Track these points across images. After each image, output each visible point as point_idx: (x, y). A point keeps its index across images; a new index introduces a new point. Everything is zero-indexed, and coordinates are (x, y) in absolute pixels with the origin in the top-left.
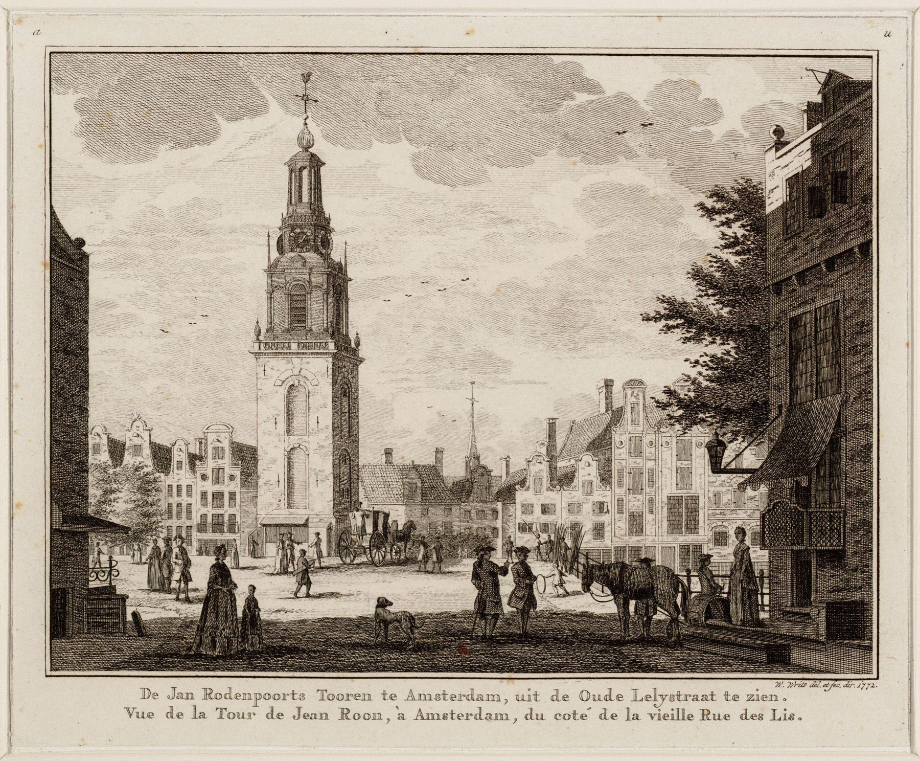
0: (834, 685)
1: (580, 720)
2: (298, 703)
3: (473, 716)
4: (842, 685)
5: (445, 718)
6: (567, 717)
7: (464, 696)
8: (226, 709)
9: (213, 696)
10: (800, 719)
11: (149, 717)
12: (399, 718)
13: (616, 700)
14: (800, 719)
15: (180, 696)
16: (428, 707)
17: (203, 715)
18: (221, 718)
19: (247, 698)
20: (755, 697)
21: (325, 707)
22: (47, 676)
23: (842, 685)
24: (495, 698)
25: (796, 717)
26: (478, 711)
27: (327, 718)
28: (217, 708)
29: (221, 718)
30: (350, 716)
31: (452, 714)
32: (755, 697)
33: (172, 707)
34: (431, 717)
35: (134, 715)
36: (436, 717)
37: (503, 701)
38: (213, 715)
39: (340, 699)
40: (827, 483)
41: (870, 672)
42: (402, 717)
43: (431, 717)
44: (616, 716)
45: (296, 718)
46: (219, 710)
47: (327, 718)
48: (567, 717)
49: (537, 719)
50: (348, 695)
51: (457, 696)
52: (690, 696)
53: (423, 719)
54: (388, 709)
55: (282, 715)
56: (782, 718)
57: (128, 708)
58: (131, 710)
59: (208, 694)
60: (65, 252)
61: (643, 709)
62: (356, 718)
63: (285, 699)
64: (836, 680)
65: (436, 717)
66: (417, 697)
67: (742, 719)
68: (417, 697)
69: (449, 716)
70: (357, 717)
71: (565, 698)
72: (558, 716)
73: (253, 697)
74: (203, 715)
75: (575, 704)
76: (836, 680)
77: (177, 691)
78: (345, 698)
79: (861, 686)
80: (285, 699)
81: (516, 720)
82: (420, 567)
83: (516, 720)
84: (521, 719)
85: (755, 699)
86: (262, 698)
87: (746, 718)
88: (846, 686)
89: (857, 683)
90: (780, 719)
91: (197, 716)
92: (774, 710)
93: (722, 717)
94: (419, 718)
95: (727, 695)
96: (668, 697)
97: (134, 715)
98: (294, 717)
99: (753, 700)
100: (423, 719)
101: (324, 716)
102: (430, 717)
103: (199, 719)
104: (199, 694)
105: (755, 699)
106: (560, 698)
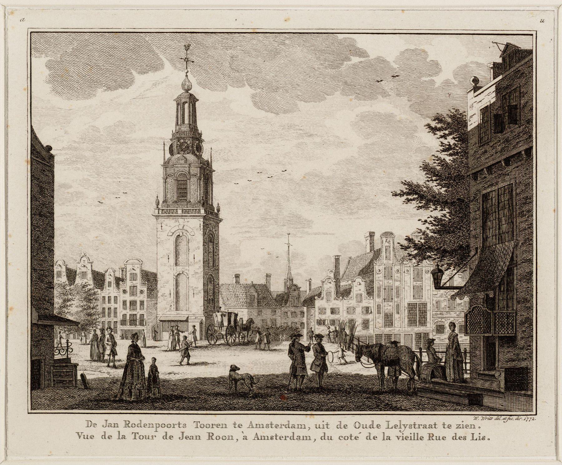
0: (509, 419)
1: (355, 440)
2: (182, 429)
4: (514, 419)
5: (272, 438)
6: (346, 438)
7: (284, 425)
8: (138, 433)
9: (130, 425)
10: (489, 439)
11: (91, 438)
12: (243, 439)
13: (376, 428)
14: (489, 439)
15: (110, 425)
16: (261, 432)
17: (124, 437)
18: (135, 438)
19: (151, 426)
20: (461, 426)
21: (199, 432)
22: (29, 413)
23: (514, 419)
24: (302, 427)
25: (486, 438)
26: (292, 435)
27: (200, 439)
28: (133, 433)
29: (135, 438)
30: (214, 437)
31: (276, 436)
32: (461, 426)
33: (105, 432)
34: (263, 438)
36: (266, 438)
37: (307, 429)
38: (130, 437)
39: (208, 427)
42: (245, 438)
43: (263, 438)
44: (377, 437)
46: (134, 434)
47: (200, 439)
48: (346, 438)
49: (328, 439)
50: (212, 425)
52: (422, 425)
53: (258, 439)
54: (237, 433)
55: (173, 437)
56: (478, 439)
57: (78, 433)
58: (80, 434)
62: (218, 438)
63: (174, 427)
64: (511, 415)
65: (266, 438)
66: (255, 426)
67: (453, 439)
68: (255, 426)
69: (274, 438)
70: (218, 438)
71: (345, 426)
72: (341, 437)
73: (154, 426)
74: (124, 437)
75: (351, 430)
76: (511, 415)
77: (108, 422)
78: (211, 426)
79: (526, 419)
80: (174, 427)
81: (315, 440)
82: (256, 346)
83: (315, 440)
84: (318, 440)
85: (461, 427)
86: (160, 427)
88: (517, 419)
89: (523, 417)
90: (476, 439)
91: (121, 437)
94: (256, 438)
95: (444, 425)
96: (408, 426)
97: (82, 437)
98: (180, 438)
99: (460, 428)
100: (258, 439)
101: (198, 437)
102: (263, 438)
103: (121, 440)
105: (461, 427)
106: (342, 427)
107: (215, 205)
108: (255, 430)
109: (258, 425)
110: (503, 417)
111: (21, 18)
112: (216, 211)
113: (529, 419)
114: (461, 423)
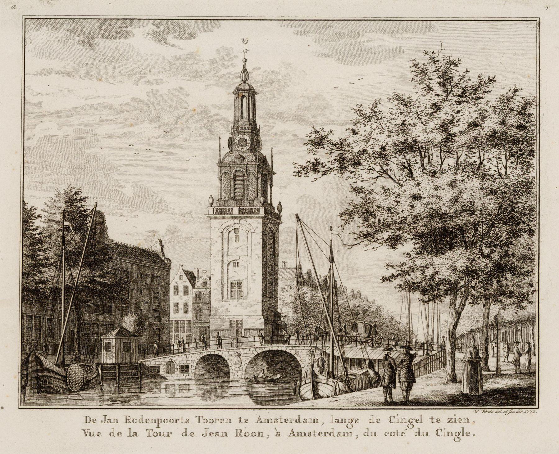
0: (510, 412)
1: (401, 436)
2: (185, 425)
3: (389, 434)
4: (515, 412)
5: (309, 435)
6: (393, 434)
9: (131, 421)
10: (474, 435)
11: (98, 436)
12: (276, 435)
13: (132, 423)
14: (474, 435)
15: (337, 421)
16: (213, 428)
17: (135, 434)
18: (149, 436)
20: (453, 420)
21: (261, 428)
22: (19, 409)
23: (515, 412)
24: (314, 421)
25: (472, 434)
26: (332, 431)
27: (226, 436)
28: (147, 430)
29: (149, 436)
30: (242, 434)
31: (314, 432)
32: (453, 420)
33: (114, 429)
34: (300, 434)
35: (88, 434)
36: (303, 434)
37: (321, 423)
38: (142, 433)
39: (172, 422)
40: (91, 331)
41: (535, 405)
42: (278, 434)
43: (300, 434)
44: (404, 433)
45: (205, 435)
47: (226, 436)
48: (393, 434)
49: (372, 436)
51: (289, 420)
53: (294, 435)
54: (106, 429)
55: (194, 434)
57: (84, 430)
58: (86, 431)
59: (127, 420)
60: (336, 295)
61: (140, 428)
62: (247, 435)
63: (216, 422)
64: (512, 409)
65: (303, 434)
67: (416, 435)
69: (312, 434)
70: (247, 434)
71: (438, 420)
72: (439, 432)
74: (135, 434)
75: (251, 427)
76: (512, 409)
77: (107, 418)
78: (175, 422)
79: (527, 412)
80: (216, 422)
81: (269, 436)
82: (505, 359)
83: (269, 436)
84: (361, 436)
86: (91, 422)
87: (114, 435)
88: (496, 412)
89: (524, 410)
91: (132, 434)
92: (130, 429)
93: (95, 434)
94: (292, 435)
95: (240, 419)
97: (88, 434)
98: (203, 435)
99: (452, 422)
100: (294, 435)
101: (224, 434)
102: (300, 434)
103: (133, 437)
104: (122, 420)
107: (275, 205)
108: (203, 425)
109: (312, 420)
110: (503, 410)
111: (13, 5)
112: (276, 211)
113: (530, 412)
114: (454, 417)
